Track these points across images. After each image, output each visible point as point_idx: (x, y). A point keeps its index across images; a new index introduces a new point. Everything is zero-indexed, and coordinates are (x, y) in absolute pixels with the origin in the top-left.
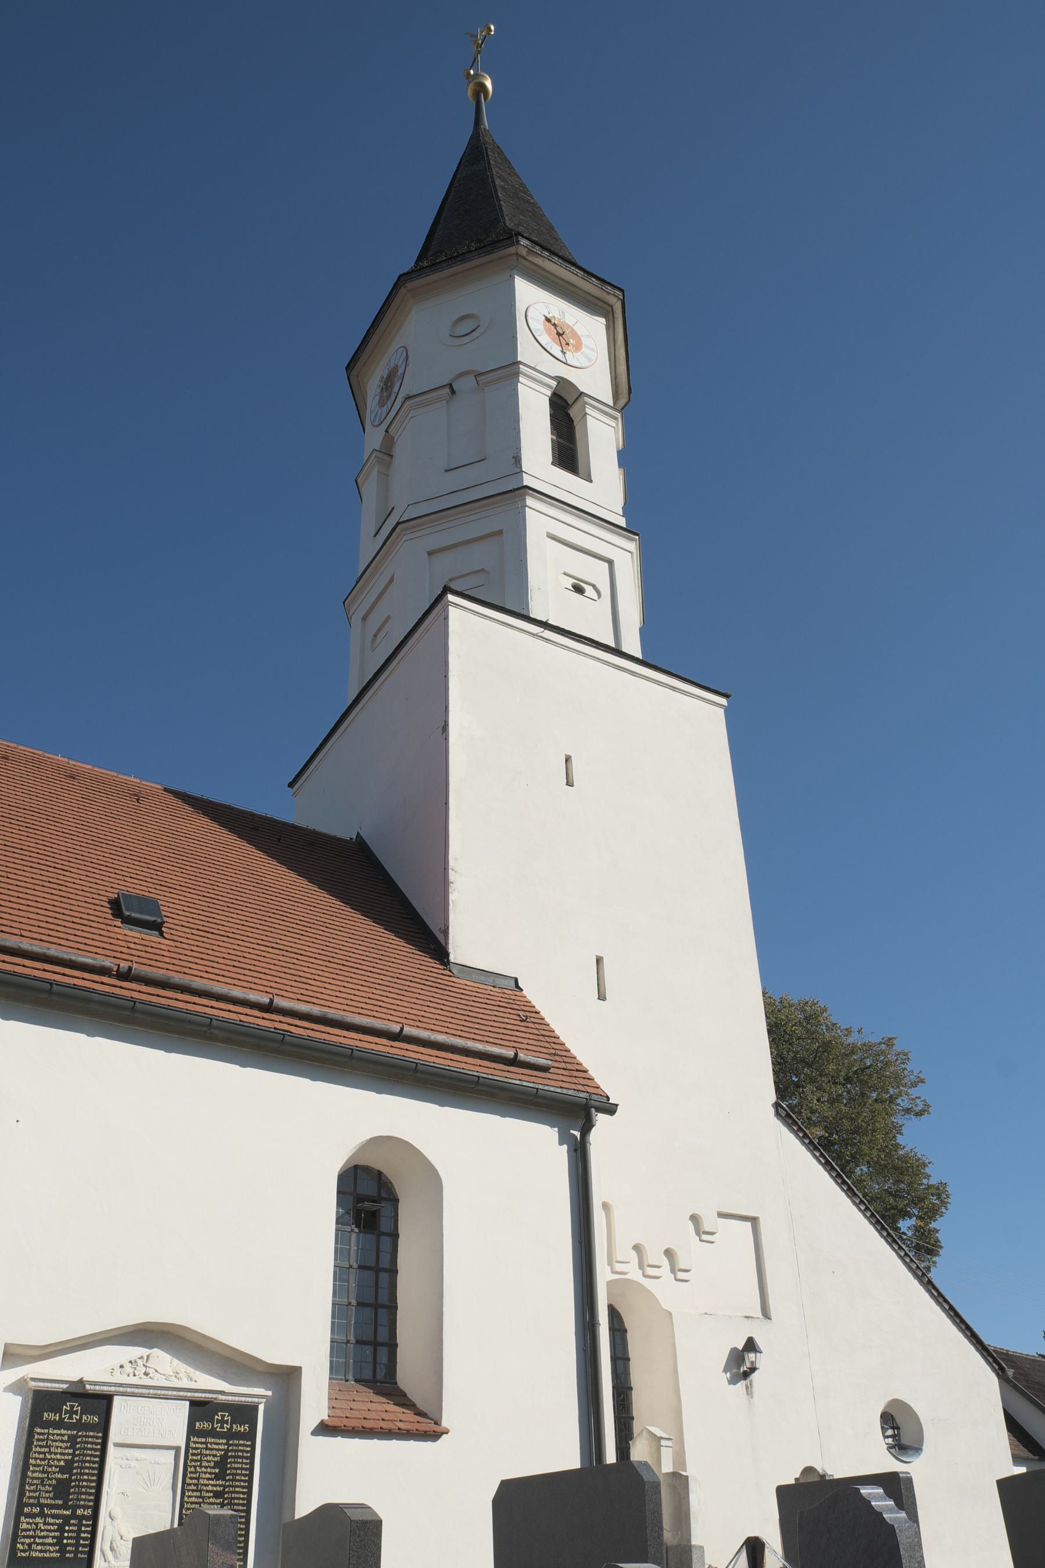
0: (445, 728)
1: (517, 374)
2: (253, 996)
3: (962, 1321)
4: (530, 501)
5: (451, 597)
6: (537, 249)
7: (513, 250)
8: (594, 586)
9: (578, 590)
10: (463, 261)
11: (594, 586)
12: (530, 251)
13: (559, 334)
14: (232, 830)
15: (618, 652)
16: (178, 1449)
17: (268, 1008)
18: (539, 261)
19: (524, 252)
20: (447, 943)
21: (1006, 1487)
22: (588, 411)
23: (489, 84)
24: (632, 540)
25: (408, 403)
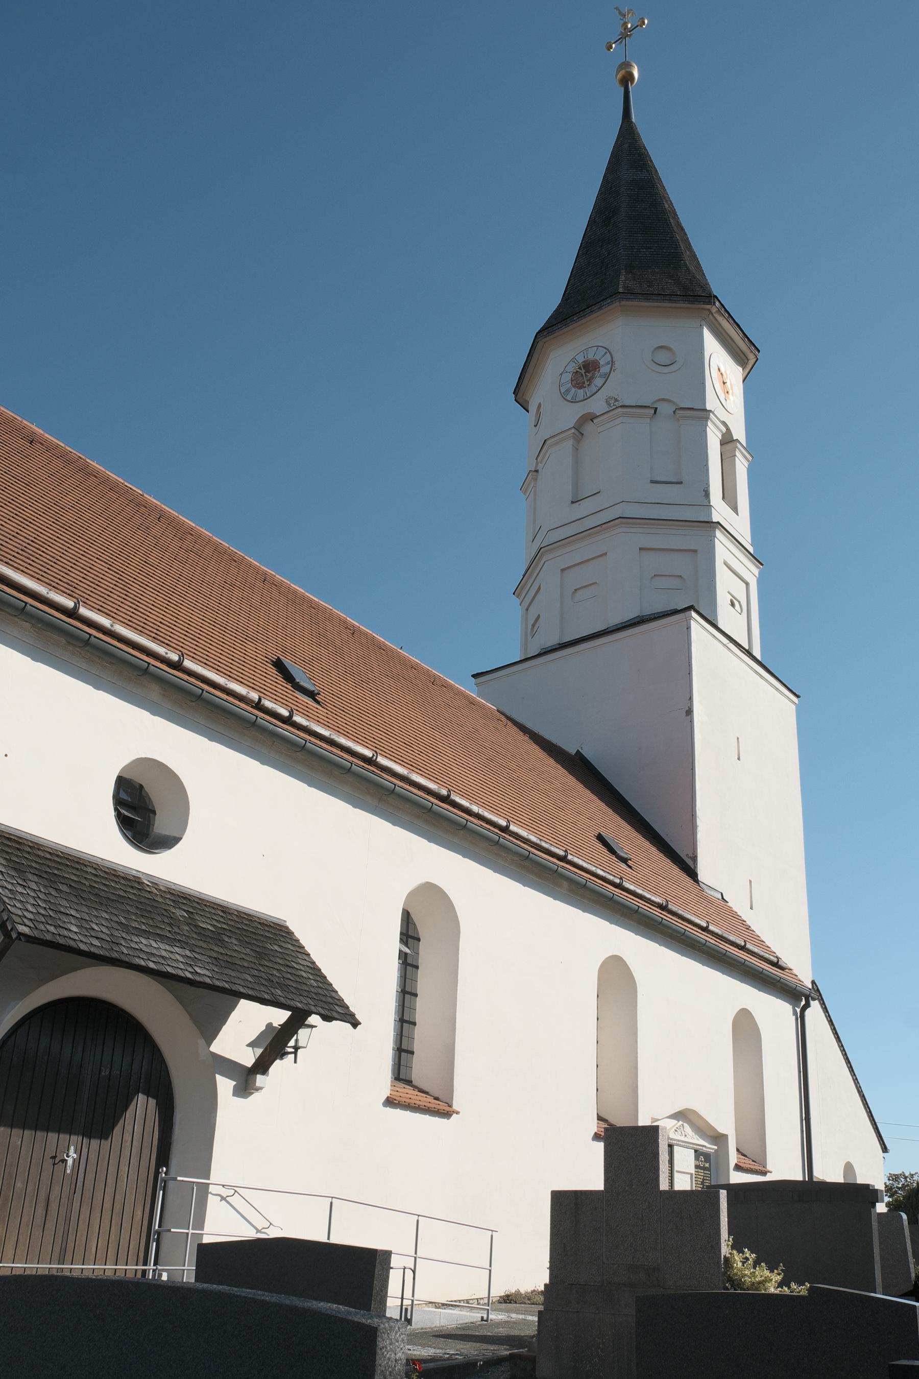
0: (689, 712)
1: (707, 418)
2: (697, 921)
3: (872, 1116)
4: (718, 534)
5: (694, 614)
6: (723, 311)
7: (708, 307)
8: (739, 602)
9: (733, 604)
10: (670, 301)
11: (739, 602)
12: (719, 311)
13: (724, 383)
14: (557, 761)
15: (749, 653)
16: (691, 1175)
17: (705, 929)
18: (720, 319)
19: (714, 310)
20: (696, 867)
21: (567, 1207)
22: (738, 453)
23: (636, 73)
24: (758, 567)
25: (620, 410)
